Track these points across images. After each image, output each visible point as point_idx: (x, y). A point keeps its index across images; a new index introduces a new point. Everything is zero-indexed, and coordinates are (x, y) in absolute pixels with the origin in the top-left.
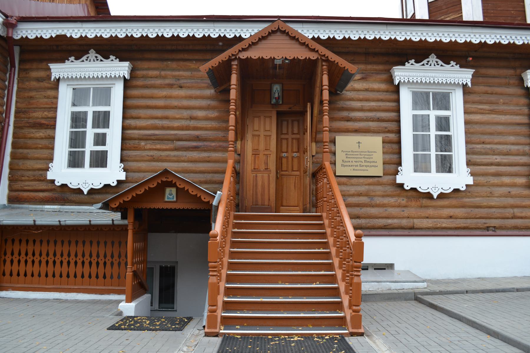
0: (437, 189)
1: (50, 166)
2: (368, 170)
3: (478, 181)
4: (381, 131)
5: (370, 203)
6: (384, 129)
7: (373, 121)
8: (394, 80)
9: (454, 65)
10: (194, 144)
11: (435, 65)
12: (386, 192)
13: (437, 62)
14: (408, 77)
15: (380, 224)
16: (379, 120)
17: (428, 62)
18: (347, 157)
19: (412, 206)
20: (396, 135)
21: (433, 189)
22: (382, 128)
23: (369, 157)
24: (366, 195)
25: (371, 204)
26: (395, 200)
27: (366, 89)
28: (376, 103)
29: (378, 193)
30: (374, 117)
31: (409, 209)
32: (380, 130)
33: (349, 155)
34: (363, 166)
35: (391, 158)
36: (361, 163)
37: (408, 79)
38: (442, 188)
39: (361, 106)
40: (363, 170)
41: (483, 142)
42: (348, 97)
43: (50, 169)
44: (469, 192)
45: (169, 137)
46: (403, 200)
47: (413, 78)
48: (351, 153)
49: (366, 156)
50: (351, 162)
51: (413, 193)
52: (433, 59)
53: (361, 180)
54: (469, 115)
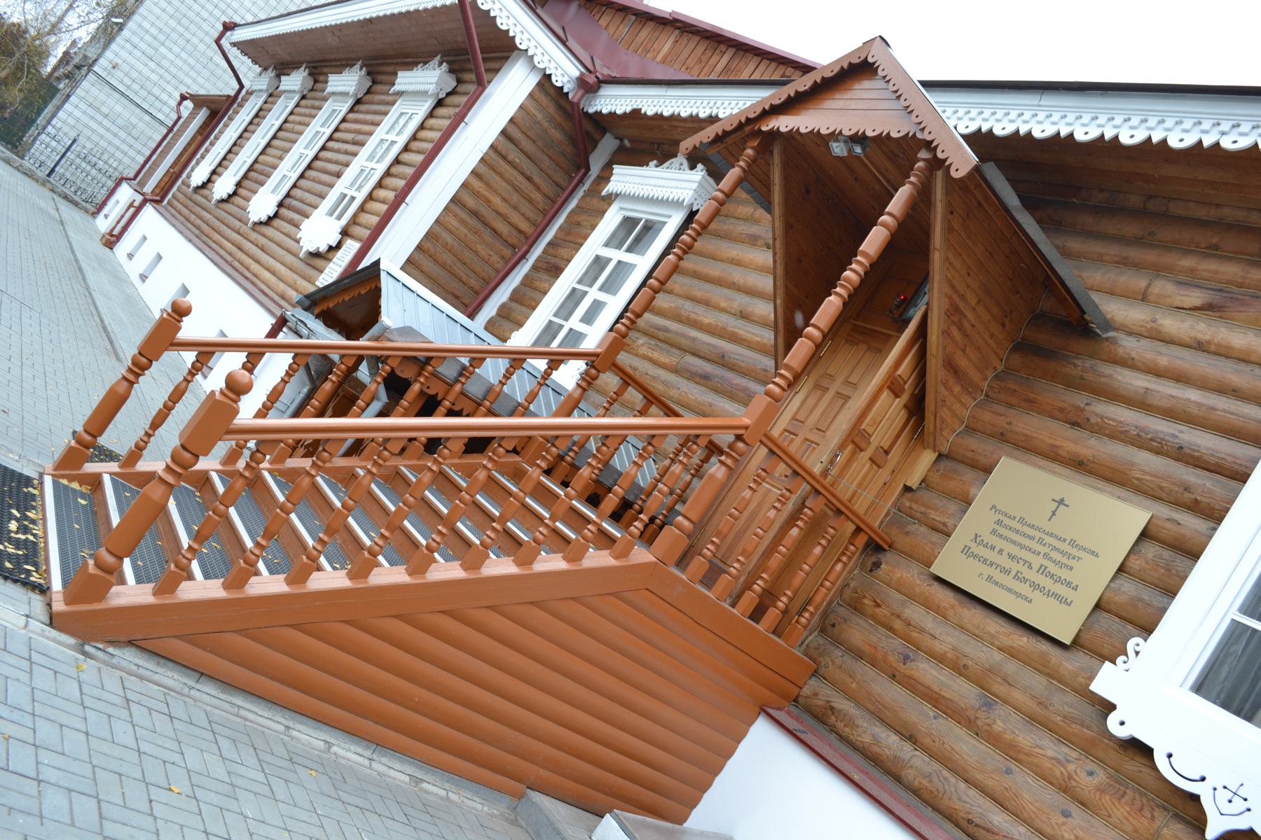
0: (1239, 805)
1: (1130, 646)
2: (1030, 602)
4: (1164, 496)
5: (971, 714)
6: (1181, 490)
7: (1158, 452)
10: (708, 367)
12: (1046, 707)
15: (958, 805)
16: (1181, 455)
18: (994, 532)
19: (1113, 819)
21: (1223, 796)
22: (1174, 484)
23: (1064, 560)
24: (980, 680)
25: (972, 718)
26: (1060, 757)
27: (1199, 343)
28: (1208, 394)
29: (1017, 695)
30: (1167, 438)
31: (1097, 823)
32: (1161, 488)
33: (1006, 527)
34: (1025, 581)
35: (1141, 600)
36: (1024, 569)
39: (1142, 391)
40: (1016, 593)
42: (1121, 351)
43: (1122, 658)
45: (683, 341)
46: (1091, 774)
48: (1014, 524)
49: (1056, 555)
50: (997, 550)
53: (994, 625)
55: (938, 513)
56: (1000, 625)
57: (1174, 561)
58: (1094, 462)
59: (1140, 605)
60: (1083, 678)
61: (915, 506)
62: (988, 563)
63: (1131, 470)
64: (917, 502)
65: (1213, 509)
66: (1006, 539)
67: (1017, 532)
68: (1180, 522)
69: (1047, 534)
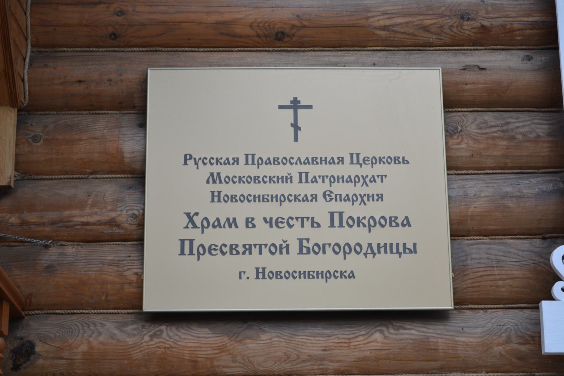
2: (352, 275)
4: (432, 38)
6: (455, 21)
18: (216, 197)
20: (529, 58)
22: (442, 15)
23: (360, 189)
32: (426, 29)
33: (229, 180)
34: (321, 248)
35: (505, 196)
36: (308, 232)
48: (242, 170)
49: (340, 189)
50: (241, 222)
55: (88, 210)
56: (322, 335)
57: (508, 123)
58: (305, 27)
59: (510, 203)
60: (499, 345)
61: (32, 217)
62: (241, 249)
63: (368, 18)
64: (31, 208)
65: (512, 31)
66: (244, 198)
67: (256, 179)
68: (482, 65)
69: (307, 162)
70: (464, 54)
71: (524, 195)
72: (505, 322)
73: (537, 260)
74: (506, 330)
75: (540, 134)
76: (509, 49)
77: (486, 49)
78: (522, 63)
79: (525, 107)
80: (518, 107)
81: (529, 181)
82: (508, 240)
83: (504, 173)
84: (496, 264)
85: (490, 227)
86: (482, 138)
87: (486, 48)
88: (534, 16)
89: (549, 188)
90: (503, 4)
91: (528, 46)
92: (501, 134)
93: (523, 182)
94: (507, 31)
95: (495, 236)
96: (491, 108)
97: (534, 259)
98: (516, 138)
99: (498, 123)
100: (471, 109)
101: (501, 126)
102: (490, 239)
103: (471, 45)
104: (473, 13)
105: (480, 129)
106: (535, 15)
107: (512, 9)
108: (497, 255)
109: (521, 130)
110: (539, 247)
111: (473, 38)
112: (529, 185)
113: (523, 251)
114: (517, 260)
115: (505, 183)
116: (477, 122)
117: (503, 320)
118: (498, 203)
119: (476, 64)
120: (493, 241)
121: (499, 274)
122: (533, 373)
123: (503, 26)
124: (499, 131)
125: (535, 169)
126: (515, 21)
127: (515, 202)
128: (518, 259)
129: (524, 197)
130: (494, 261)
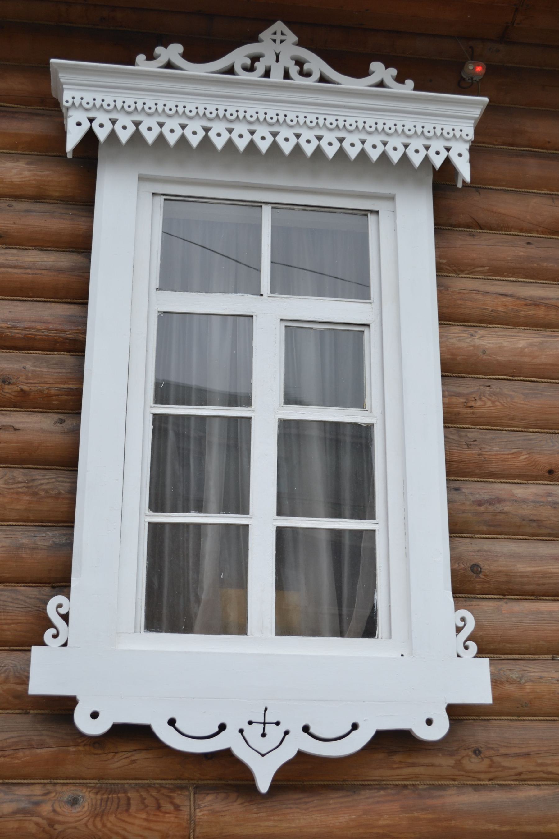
0: (275, 733)
3: (529, 686)
8: (65, 125)
9: (389, 81)
11: (287, 75)
13: (300, 63)
14: (137, 118)
17: (255, 59)
20: (62, 421)
26: (24, 805)
35: (21, 547)
37: (132, 129)
38: (306, 729)
41: (551, 472)
44: (477, 752)
46: (74, 802)
47: (161, 125)
51: (137, 756)
52: (278, 47)
54: (472, 330)
57: (34, 480)
59: (24, 554)
65: (49, 396)
68: (17, 426)
70: (3, 414)
71: (38, 547)
72: (6, 663)
73: (41, 607)
74: (6, 670)
75: (61, 491)
76: (46, 412)
77: (25, 411)
78: (53, 426)
79: (54, 466)
80: (48, 466)
81: (47, 534)
82: (20, 587)
83: (26, 526)
84: (3, 609)
85: (4, 575)
86: (7, 493)
87: (26, 410)
88: (70, 384)
89: (63, 541)
90: (43, 371)
91: (64, 410)
92: (25, 490)
93: (40, 534)
94: (44, 396)
95: (9, 583)
96: (23, 465)
97: (39, 606)
98: (39, 494)
99: (25, 479)
100: (4, 465)
101: (27, 483)
102: (4, 586)
103: (12, 406)
104: (14, 379)
105: (7, 484)
106: (70, 383)
107: (49, 377)
108: (6, 601)
109: (44, 487)
110: (46, 595)
111: (13, 400)
112: (45, 538)
113: (31, 598)
114: (23, 607)
115: (23, 535)
116: (6, 478)
117: (5, 661)
118: (12, 554)
119: (12, 424)
120: (6, 587)
121: (5, 619)
122: (28, 711)
123: (41, 391)
124: (24, 487)
125: (55, 523)
126: (52, 387)
127: (29, 553)
128: (25, 605)
129: (38, 549)
130: (2, 607)
